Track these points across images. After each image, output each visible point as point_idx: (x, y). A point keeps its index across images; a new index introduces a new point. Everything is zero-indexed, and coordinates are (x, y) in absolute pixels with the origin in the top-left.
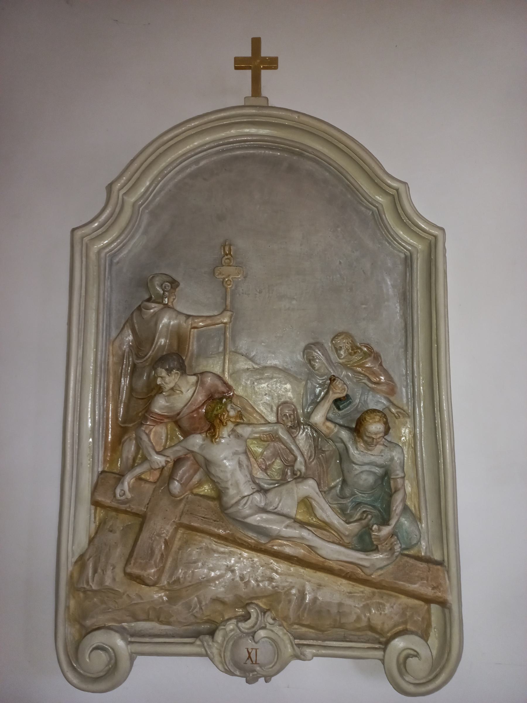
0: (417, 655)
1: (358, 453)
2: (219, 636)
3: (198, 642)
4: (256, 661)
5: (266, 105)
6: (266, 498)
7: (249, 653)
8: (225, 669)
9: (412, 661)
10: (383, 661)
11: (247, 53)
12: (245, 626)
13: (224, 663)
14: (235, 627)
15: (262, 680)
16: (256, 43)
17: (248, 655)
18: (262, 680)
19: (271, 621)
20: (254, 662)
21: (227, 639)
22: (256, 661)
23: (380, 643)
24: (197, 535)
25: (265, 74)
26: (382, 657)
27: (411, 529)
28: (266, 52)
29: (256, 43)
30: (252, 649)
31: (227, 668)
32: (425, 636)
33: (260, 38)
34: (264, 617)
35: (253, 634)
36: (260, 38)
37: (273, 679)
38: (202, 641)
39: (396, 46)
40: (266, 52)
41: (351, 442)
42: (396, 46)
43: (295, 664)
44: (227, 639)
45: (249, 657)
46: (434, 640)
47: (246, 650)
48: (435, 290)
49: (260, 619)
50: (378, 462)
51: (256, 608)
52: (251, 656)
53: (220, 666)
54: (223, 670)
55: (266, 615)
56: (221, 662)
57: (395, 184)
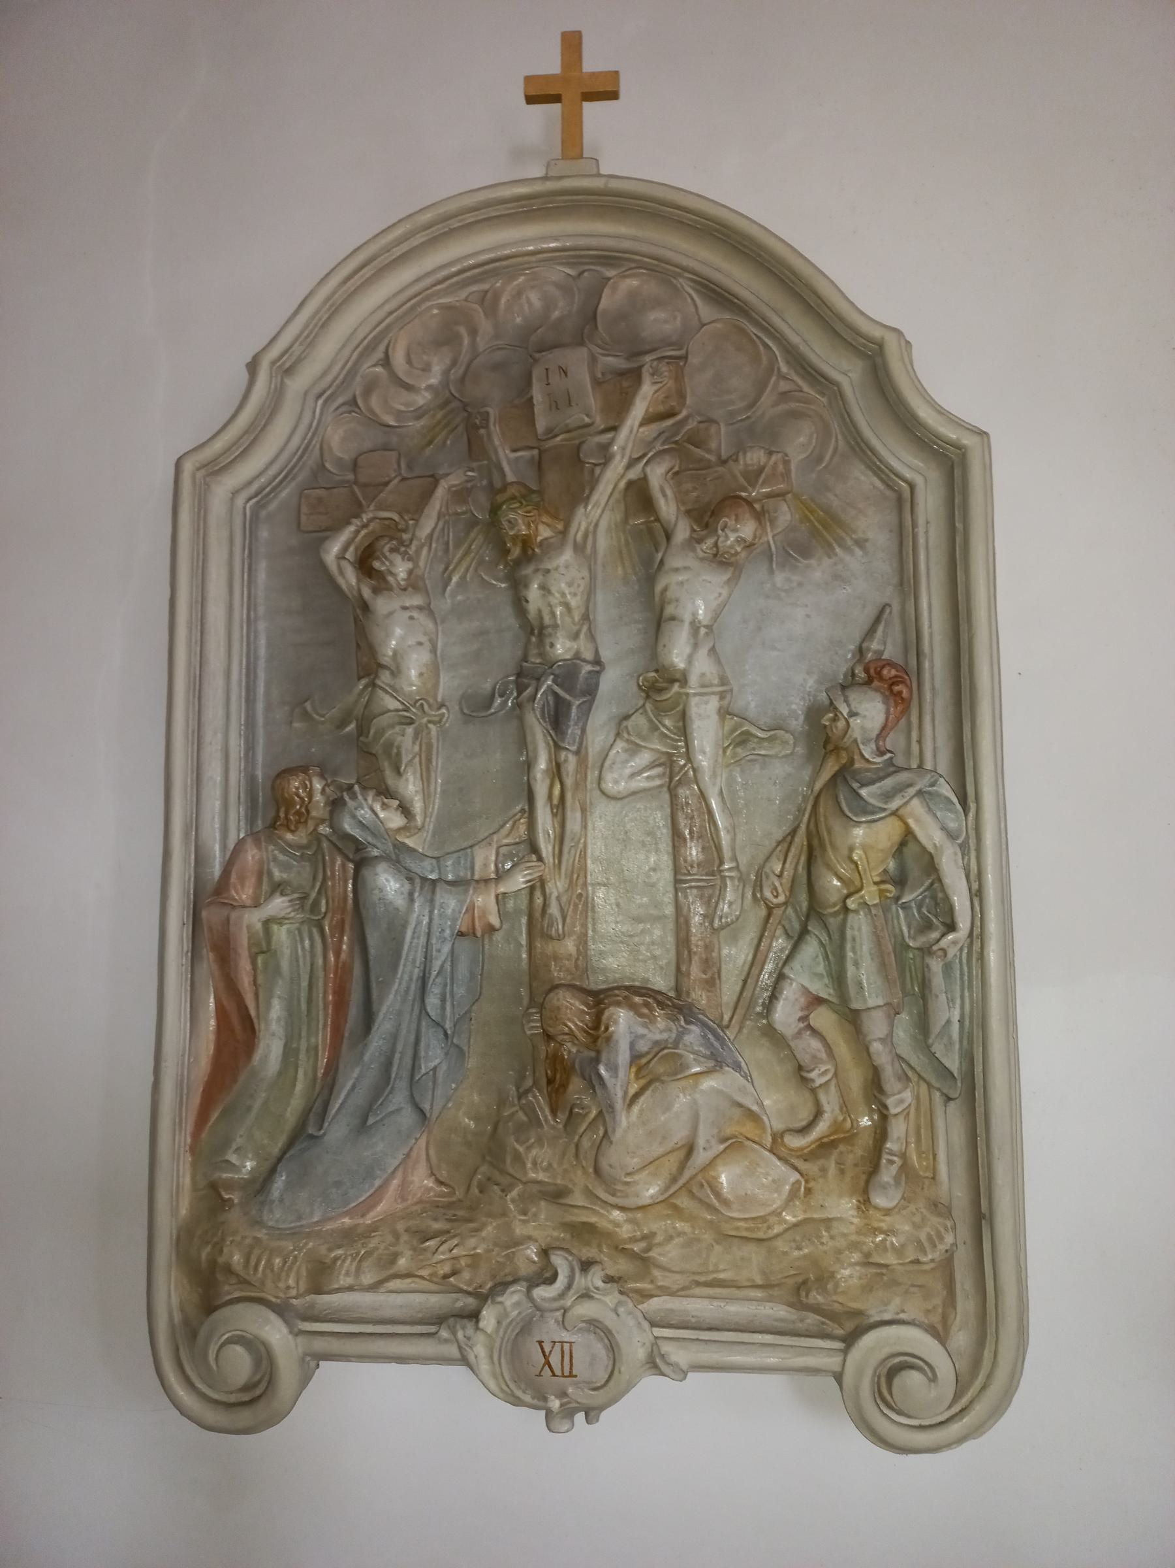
2: (489, 1318)
3: (444, 1334)
9: (913, 1378)
10: (839, 1377)
11: (550, 64)
14: (524, 1299)
15: (580, 1417)
16: (572, 43)
17: (543, 1360)
18: (580, 1417)
19: (600, 1284)
21: (504, 1324)
25: (592, 111)
26: (838, 1369)
28: (593, 62)
29: (572, 43)
33: (617, 72)
36: (617, 72)
37: (605, 1415)
38: (454, 1332)
40: (593, 62)
43: (651, 1384)
44: (504, 1324)
45: (548, 1363)
46: (961, 1338)
48: (729, 293)
50: (731, 522)
52: (551, 1360)
53: (492, 1384)
56: (494, 1376)
57: (952, 434)
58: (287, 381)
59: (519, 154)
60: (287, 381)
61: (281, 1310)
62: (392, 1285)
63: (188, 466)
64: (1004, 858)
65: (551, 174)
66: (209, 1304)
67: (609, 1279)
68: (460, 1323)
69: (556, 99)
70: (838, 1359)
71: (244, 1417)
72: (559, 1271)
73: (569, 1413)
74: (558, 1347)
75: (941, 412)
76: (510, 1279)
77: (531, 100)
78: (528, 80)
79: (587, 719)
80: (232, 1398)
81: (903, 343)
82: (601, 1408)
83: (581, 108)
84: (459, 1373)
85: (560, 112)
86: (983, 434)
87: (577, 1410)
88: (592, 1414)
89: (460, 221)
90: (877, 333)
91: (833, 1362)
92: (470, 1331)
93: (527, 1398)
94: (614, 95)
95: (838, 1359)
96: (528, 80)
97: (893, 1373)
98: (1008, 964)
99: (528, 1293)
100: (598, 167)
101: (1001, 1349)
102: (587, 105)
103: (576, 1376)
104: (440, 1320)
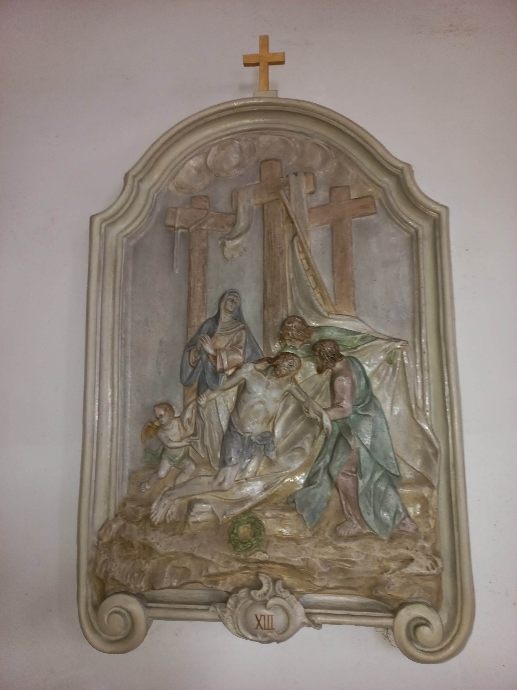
0: (427, 623)
1: (216, 153)
4: (272, 627)
5: (275, 96)
7: (259, 621)
9: (424, 631)
11: (255, 49)
12: (257, 594)
13: (236, 628)
16: (264, 41)
17: (256, 622)
22: (272, 627)
24: (286, 534)
27: (412, 398)
28: (273, 48)
29: (264, 41)
30: (261, 615)
32: (435, 607)
33: (284, 53)
35: (264, 603)
39: (503, 666)
40: (273, 48)
42: (503, 666)
43: (307, 632)
45: (259, 624)
46: (444, 615)
47: (255, 617)
51: (268, 577)
58: (140, 184)
59: (243, 88)
60: (140, 184)
62: (188, 586)
63: (97, 221)
65: (256, 96)
66: (103, 596)
69: (257, 64)
74: (263, 617)
75: (422, 193)
77: (246, 65)
78: (244, 57)
79: (251, 334)
84: (220, 624)
86: (446, 208)
89: (408, 227)
93: (250, 637)
94: (282, 63)
96: (244, 57)
97: (417, 626)
99: (249, 594)
100: (277, 94)
102: (271, 67)
103: (274, 629)
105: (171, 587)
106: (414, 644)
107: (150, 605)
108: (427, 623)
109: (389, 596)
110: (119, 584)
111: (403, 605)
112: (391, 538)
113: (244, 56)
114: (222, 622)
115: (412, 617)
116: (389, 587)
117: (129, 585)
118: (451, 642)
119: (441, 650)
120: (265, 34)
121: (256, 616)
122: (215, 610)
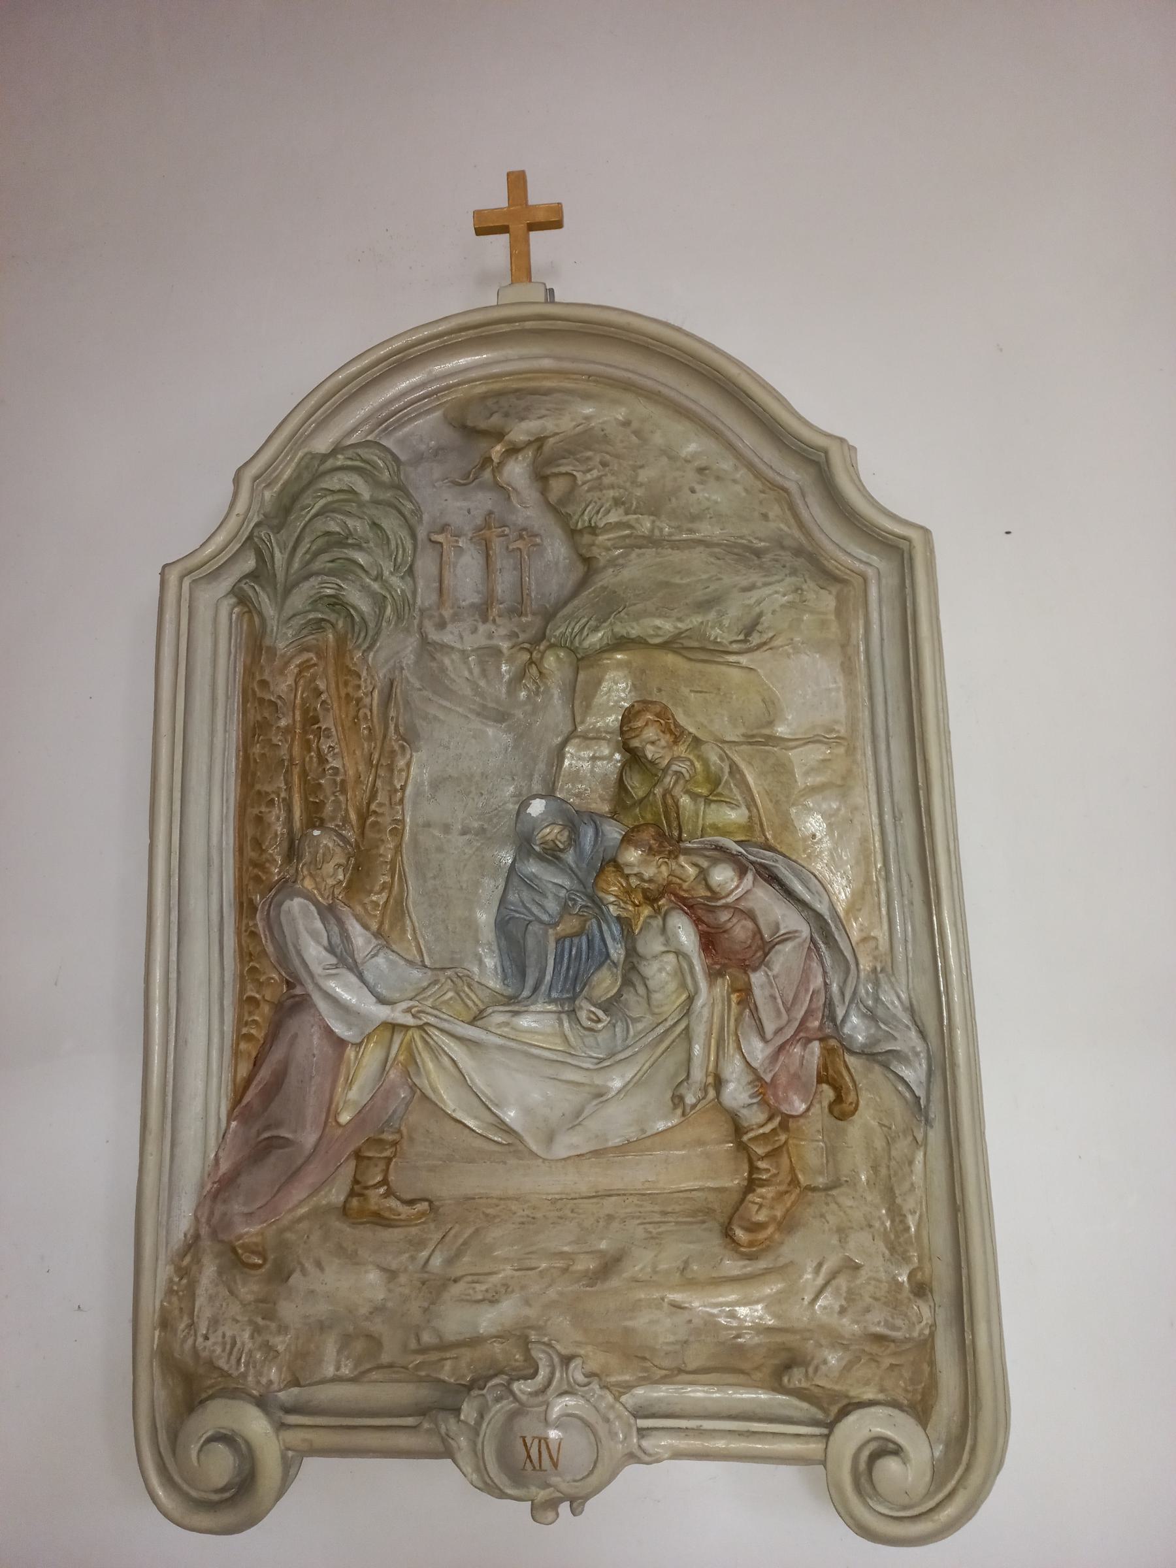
0: (897, 1451)
6: (707, 742)
8: (485, 1483)
9: (891, 1465)
10: (751, 1185)
11: (497, 198)
13: (481, 1468)
15: (564, 1508)
16: (517, 182)
18: (564, 1508)
20: (538, 1468)
23: (815, 1423)
25: (537, 238)
28: (538, 195)
29: (517, 182)
31: (489, 1481)
34: (567, 1369)
37: (590, 1504)
40: (538, 195)
41: (500, 1357)
45: (529, 1457)
49: (558, 1375)
50: (723, 1118)
54: (480, 1485)
55: (572, 1365)
57: (898, 529)
61: (261, 1403)
64: (984, 1196)
67: (590, 1375)
68: (441, 1416)
69: (504, 229)
70: (821, 1446)
71: (227, 1517)
72: (541, 1366)
73: (552, 1504)
76: (491, 1372)
77: (480, 231)
78: (478, 214)
80: (216, 1497)
81: (846, 450)
82: (586, 1498)
83: (527, 241)
85: (502, 206)
87: (561, 1500)
88: (577, 1503)
90: (821, 441)
91: (814, 1448)
92: (452, 1421)
94: (558, 225)
95: (821, 1446)
96: (478, 214)
97: (874, 1457)
98: (966, 978)
101: (980, 1439)
104: (423, 1411)
105: (337, 1379)
106: (869, 1500)
107: (292, 1419)
108: (897, 1451)
109: (816, 1390)
110: (222, 1376)
111: (850, 1407)
112: (517, 1476)
113: (508, 174)
114: (450, 1460)
115: (872, 1435)
116: (816, 1369)
117: (244, 1376)
118: (951, 1495)
119: (939, 1506)
120: (516, 168)
121: (524, 1438)
122: (432, 1426)
